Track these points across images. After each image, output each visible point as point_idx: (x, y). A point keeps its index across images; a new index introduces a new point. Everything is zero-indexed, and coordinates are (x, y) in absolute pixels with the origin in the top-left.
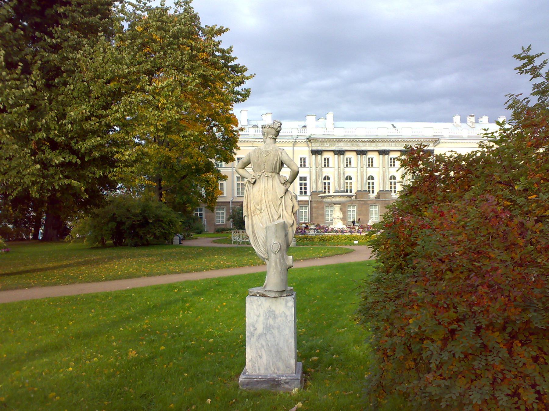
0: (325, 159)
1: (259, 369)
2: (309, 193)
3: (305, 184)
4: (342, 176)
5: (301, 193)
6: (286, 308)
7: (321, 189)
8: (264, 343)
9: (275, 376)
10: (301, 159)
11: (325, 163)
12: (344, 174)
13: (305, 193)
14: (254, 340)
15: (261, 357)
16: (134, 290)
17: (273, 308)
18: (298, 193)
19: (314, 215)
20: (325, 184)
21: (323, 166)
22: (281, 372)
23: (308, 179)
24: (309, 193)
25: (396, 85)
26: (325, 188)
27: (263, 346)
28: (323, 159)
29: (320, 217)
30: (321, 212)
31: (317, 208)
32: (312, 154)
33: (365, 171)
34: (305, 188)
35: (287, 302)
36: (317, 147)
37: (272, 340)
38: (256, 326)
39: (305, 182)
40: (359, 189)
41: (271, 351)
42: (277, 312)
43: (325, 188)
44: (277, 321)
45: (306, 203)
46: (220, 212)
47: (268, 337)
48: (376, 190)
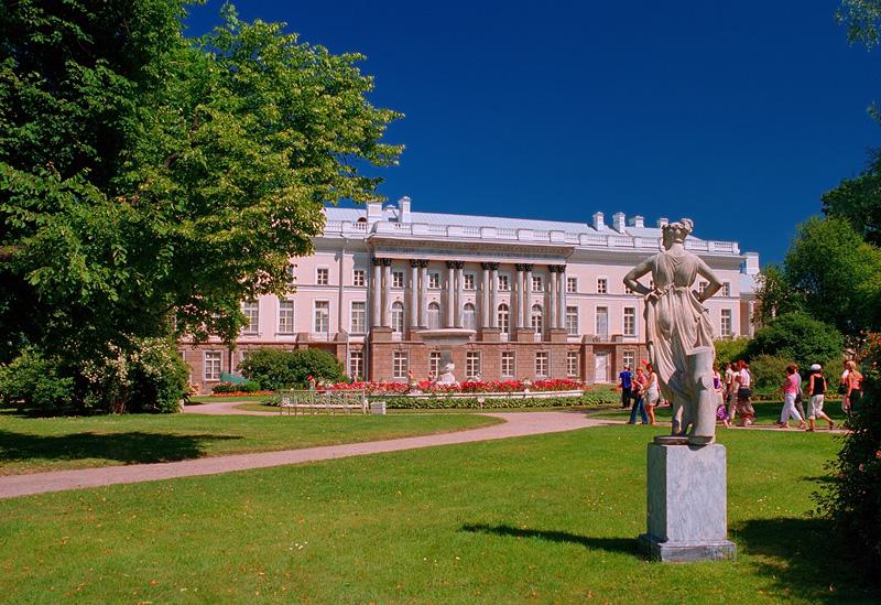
0: (569, 280)
3: (632, 319)
10: (319, 271)
35: (718, 450)
37: (700, 499)
38: (680, 482)
41: (697, 513)
42: (705, 464)
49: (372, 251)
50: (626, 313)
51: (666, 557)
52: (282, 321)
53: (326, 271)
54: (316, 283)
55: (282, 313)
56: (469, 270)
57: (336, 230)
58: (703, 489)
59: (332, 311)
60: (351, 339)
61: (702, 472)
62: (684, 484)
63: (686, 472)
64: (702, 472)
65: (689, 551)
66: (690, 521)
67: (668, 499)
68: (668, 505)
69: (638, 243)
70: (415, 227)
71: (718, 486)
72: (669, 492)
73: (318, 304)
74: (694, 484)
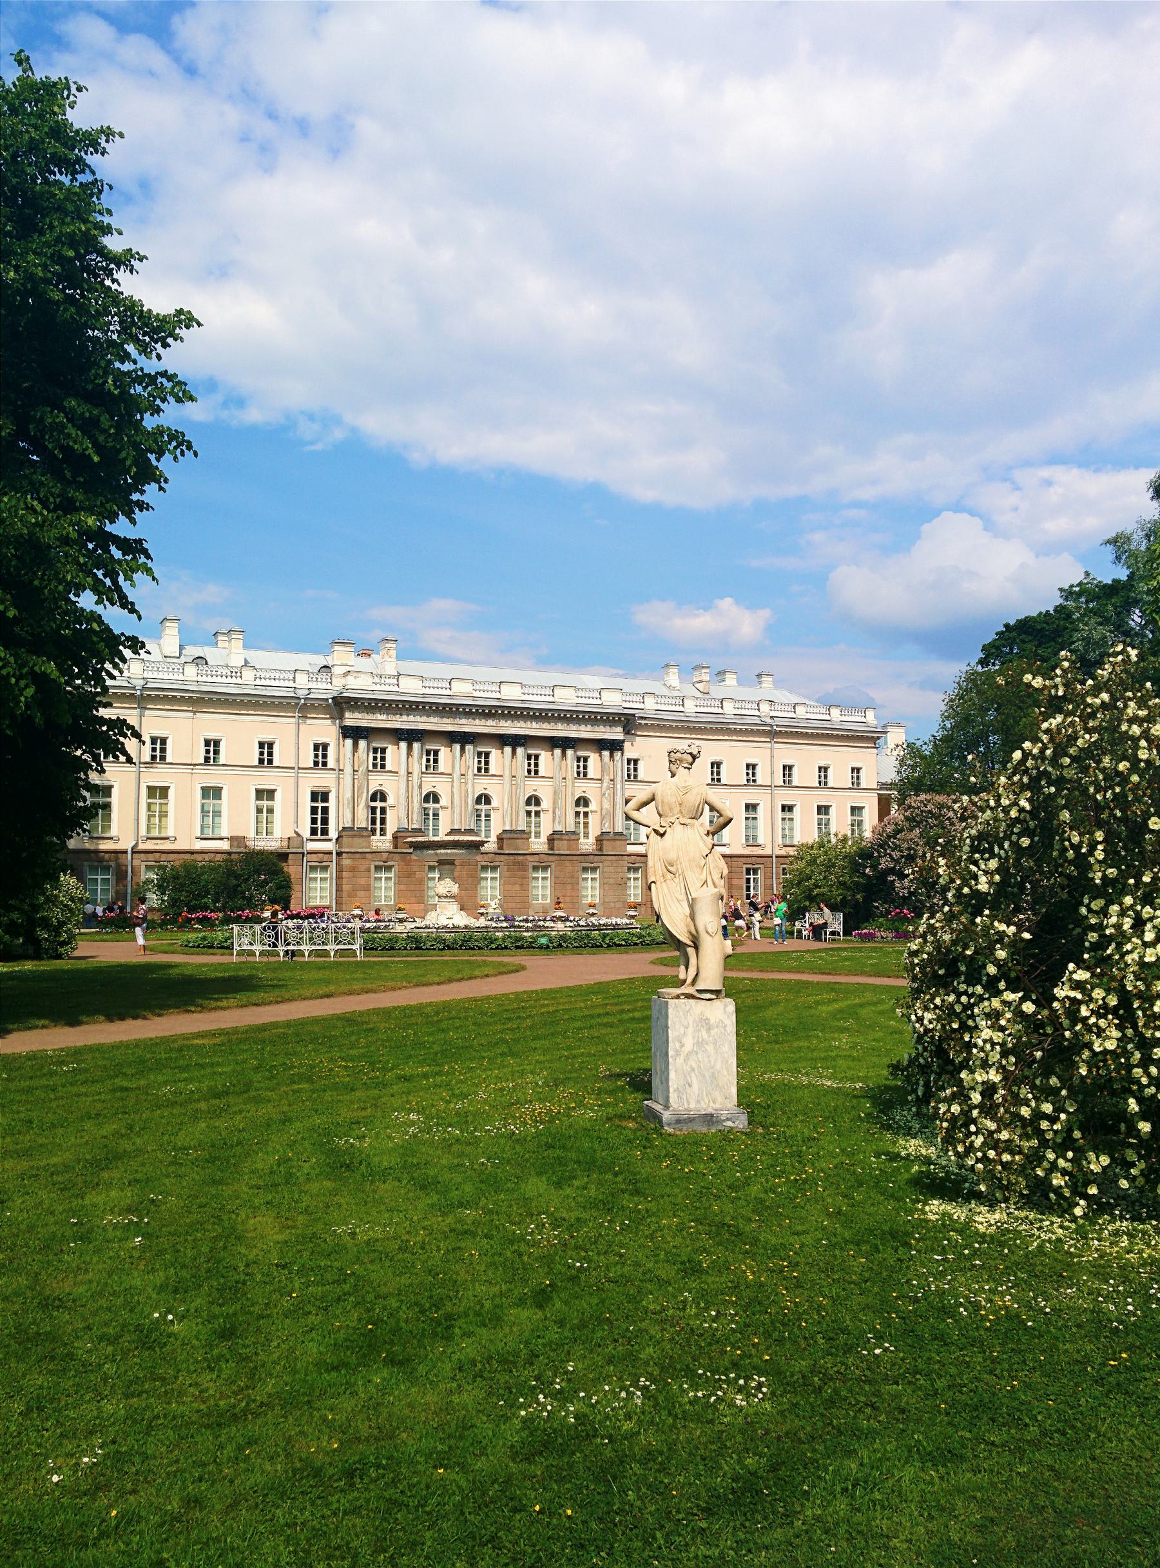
0: (629, 761)
1: (688, 1103)
2: (333, 834)
3: (325, 810)
4: (416, 791)
5: (314, 832)
6: (724, 1012)
7: (363, 821)
8: (694, 1065)
9: (710, 1111)
10: (261, 745)
11: (629, 770)
12: (420, 787)
13: (325, 832)
14: (680, 1061)
15: (690, 1086)
16: (376, 1012)
17: (708, 1014)
18: (306, 833)
19: (346, 888)
20: (374, 810)
21: (371, 768)
22: (718, 1106)
23: (332, 797)
24: (333, 834)
25: (446, 974)
26: (374, 821)
27: (693, 1070)
28: (626, 762)
29: (361, 893)
30: (362, 881)
31: (353, 869)
32: (345, 736)
33: (470, 785)
34: (325, 821)
35: (725, 1006)
36: (354, 719)
37: (706, 1059)
38: (684, 1040)
39: (270, 803)
40: (508, 828)
41: (704, 1076)
42: (712, 1021)
43: (374, 821)
44: (712, 1032)
45: (326, 857)
46: (99, 877)
47: (700, 1056)
48: (391, 828)
49: (342, 717)
50: (258, 798)
51: (669, 1125)
52: (314, 821)
53: (754, 766)
54: (257, 763)
55: (314, 810)
56: (533, 747)
57: (286, 684)
58: (710, 1048)
59: (761, 812)
60: (311, 846)
61: (709, 1030)
62: (689, 1043)
63: (690, 1030)
64: (709, 1030)
65: (694, 1119)
66: (695, 1085)
67: (670, 1060)
68: (670, 1067)
69: (729, 708)
70: (402, 680)
71: (727, 1046)
72: (671, 1053)
73: (260, 794)
74: (700, 1043)
